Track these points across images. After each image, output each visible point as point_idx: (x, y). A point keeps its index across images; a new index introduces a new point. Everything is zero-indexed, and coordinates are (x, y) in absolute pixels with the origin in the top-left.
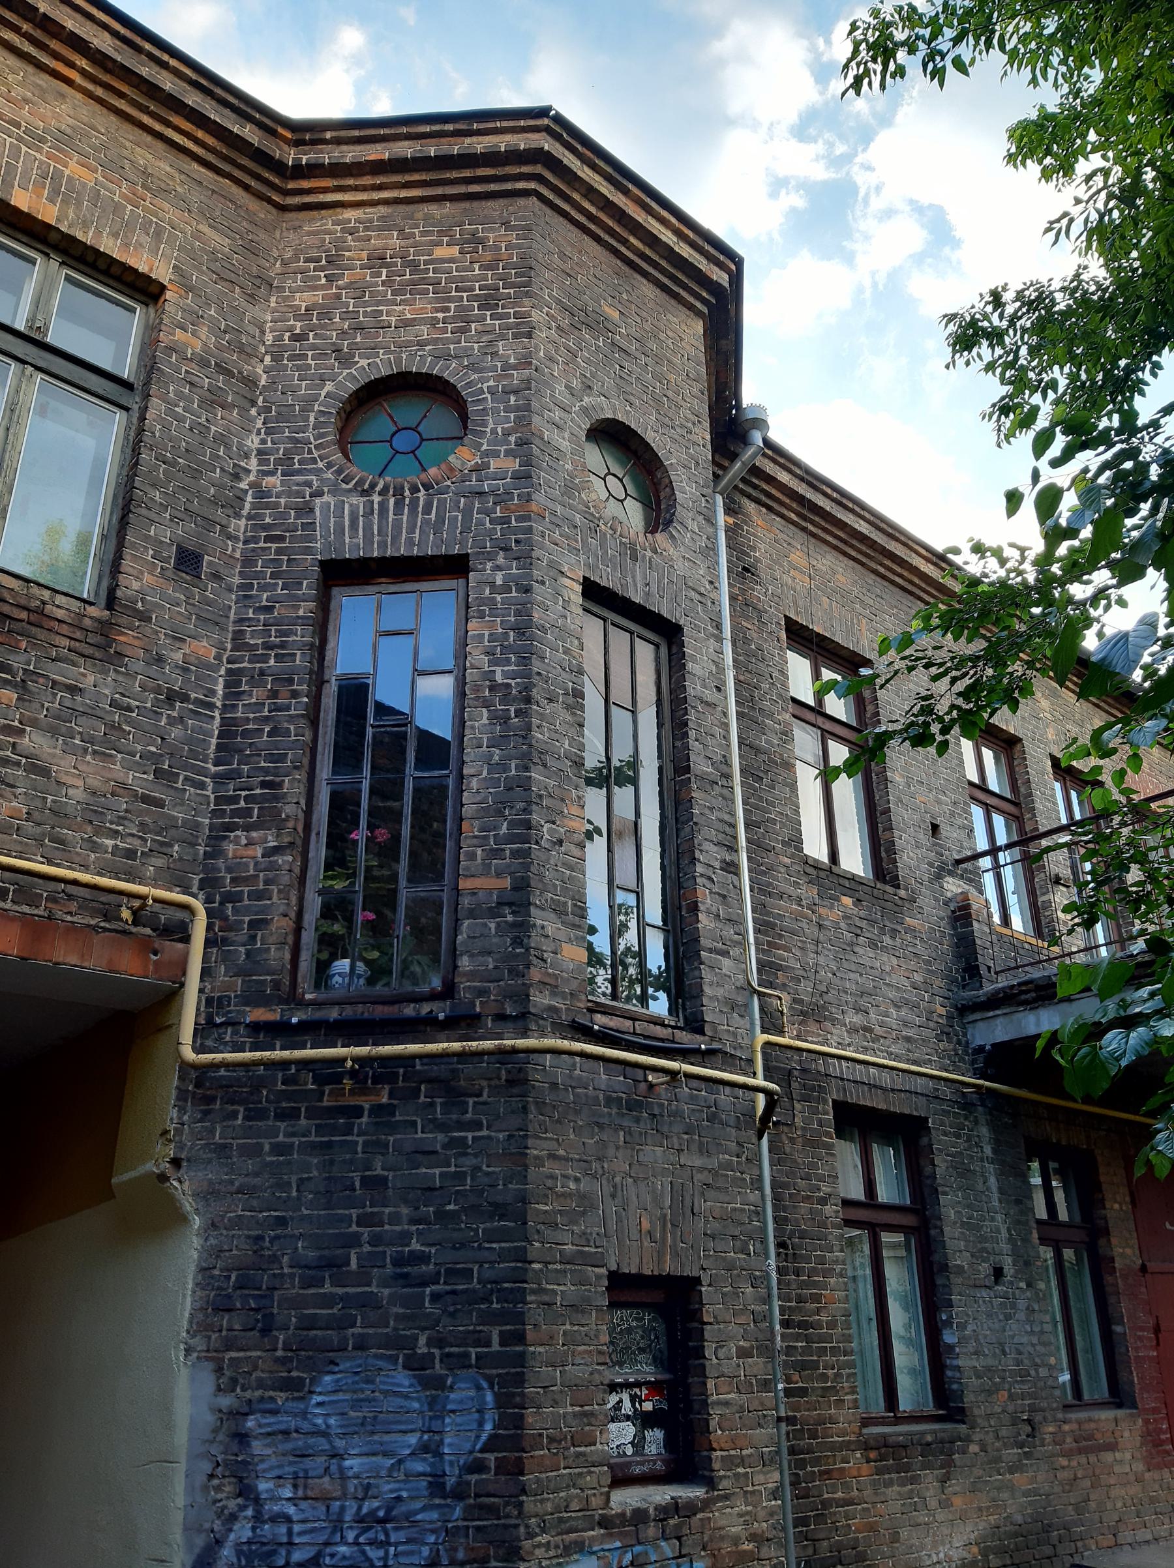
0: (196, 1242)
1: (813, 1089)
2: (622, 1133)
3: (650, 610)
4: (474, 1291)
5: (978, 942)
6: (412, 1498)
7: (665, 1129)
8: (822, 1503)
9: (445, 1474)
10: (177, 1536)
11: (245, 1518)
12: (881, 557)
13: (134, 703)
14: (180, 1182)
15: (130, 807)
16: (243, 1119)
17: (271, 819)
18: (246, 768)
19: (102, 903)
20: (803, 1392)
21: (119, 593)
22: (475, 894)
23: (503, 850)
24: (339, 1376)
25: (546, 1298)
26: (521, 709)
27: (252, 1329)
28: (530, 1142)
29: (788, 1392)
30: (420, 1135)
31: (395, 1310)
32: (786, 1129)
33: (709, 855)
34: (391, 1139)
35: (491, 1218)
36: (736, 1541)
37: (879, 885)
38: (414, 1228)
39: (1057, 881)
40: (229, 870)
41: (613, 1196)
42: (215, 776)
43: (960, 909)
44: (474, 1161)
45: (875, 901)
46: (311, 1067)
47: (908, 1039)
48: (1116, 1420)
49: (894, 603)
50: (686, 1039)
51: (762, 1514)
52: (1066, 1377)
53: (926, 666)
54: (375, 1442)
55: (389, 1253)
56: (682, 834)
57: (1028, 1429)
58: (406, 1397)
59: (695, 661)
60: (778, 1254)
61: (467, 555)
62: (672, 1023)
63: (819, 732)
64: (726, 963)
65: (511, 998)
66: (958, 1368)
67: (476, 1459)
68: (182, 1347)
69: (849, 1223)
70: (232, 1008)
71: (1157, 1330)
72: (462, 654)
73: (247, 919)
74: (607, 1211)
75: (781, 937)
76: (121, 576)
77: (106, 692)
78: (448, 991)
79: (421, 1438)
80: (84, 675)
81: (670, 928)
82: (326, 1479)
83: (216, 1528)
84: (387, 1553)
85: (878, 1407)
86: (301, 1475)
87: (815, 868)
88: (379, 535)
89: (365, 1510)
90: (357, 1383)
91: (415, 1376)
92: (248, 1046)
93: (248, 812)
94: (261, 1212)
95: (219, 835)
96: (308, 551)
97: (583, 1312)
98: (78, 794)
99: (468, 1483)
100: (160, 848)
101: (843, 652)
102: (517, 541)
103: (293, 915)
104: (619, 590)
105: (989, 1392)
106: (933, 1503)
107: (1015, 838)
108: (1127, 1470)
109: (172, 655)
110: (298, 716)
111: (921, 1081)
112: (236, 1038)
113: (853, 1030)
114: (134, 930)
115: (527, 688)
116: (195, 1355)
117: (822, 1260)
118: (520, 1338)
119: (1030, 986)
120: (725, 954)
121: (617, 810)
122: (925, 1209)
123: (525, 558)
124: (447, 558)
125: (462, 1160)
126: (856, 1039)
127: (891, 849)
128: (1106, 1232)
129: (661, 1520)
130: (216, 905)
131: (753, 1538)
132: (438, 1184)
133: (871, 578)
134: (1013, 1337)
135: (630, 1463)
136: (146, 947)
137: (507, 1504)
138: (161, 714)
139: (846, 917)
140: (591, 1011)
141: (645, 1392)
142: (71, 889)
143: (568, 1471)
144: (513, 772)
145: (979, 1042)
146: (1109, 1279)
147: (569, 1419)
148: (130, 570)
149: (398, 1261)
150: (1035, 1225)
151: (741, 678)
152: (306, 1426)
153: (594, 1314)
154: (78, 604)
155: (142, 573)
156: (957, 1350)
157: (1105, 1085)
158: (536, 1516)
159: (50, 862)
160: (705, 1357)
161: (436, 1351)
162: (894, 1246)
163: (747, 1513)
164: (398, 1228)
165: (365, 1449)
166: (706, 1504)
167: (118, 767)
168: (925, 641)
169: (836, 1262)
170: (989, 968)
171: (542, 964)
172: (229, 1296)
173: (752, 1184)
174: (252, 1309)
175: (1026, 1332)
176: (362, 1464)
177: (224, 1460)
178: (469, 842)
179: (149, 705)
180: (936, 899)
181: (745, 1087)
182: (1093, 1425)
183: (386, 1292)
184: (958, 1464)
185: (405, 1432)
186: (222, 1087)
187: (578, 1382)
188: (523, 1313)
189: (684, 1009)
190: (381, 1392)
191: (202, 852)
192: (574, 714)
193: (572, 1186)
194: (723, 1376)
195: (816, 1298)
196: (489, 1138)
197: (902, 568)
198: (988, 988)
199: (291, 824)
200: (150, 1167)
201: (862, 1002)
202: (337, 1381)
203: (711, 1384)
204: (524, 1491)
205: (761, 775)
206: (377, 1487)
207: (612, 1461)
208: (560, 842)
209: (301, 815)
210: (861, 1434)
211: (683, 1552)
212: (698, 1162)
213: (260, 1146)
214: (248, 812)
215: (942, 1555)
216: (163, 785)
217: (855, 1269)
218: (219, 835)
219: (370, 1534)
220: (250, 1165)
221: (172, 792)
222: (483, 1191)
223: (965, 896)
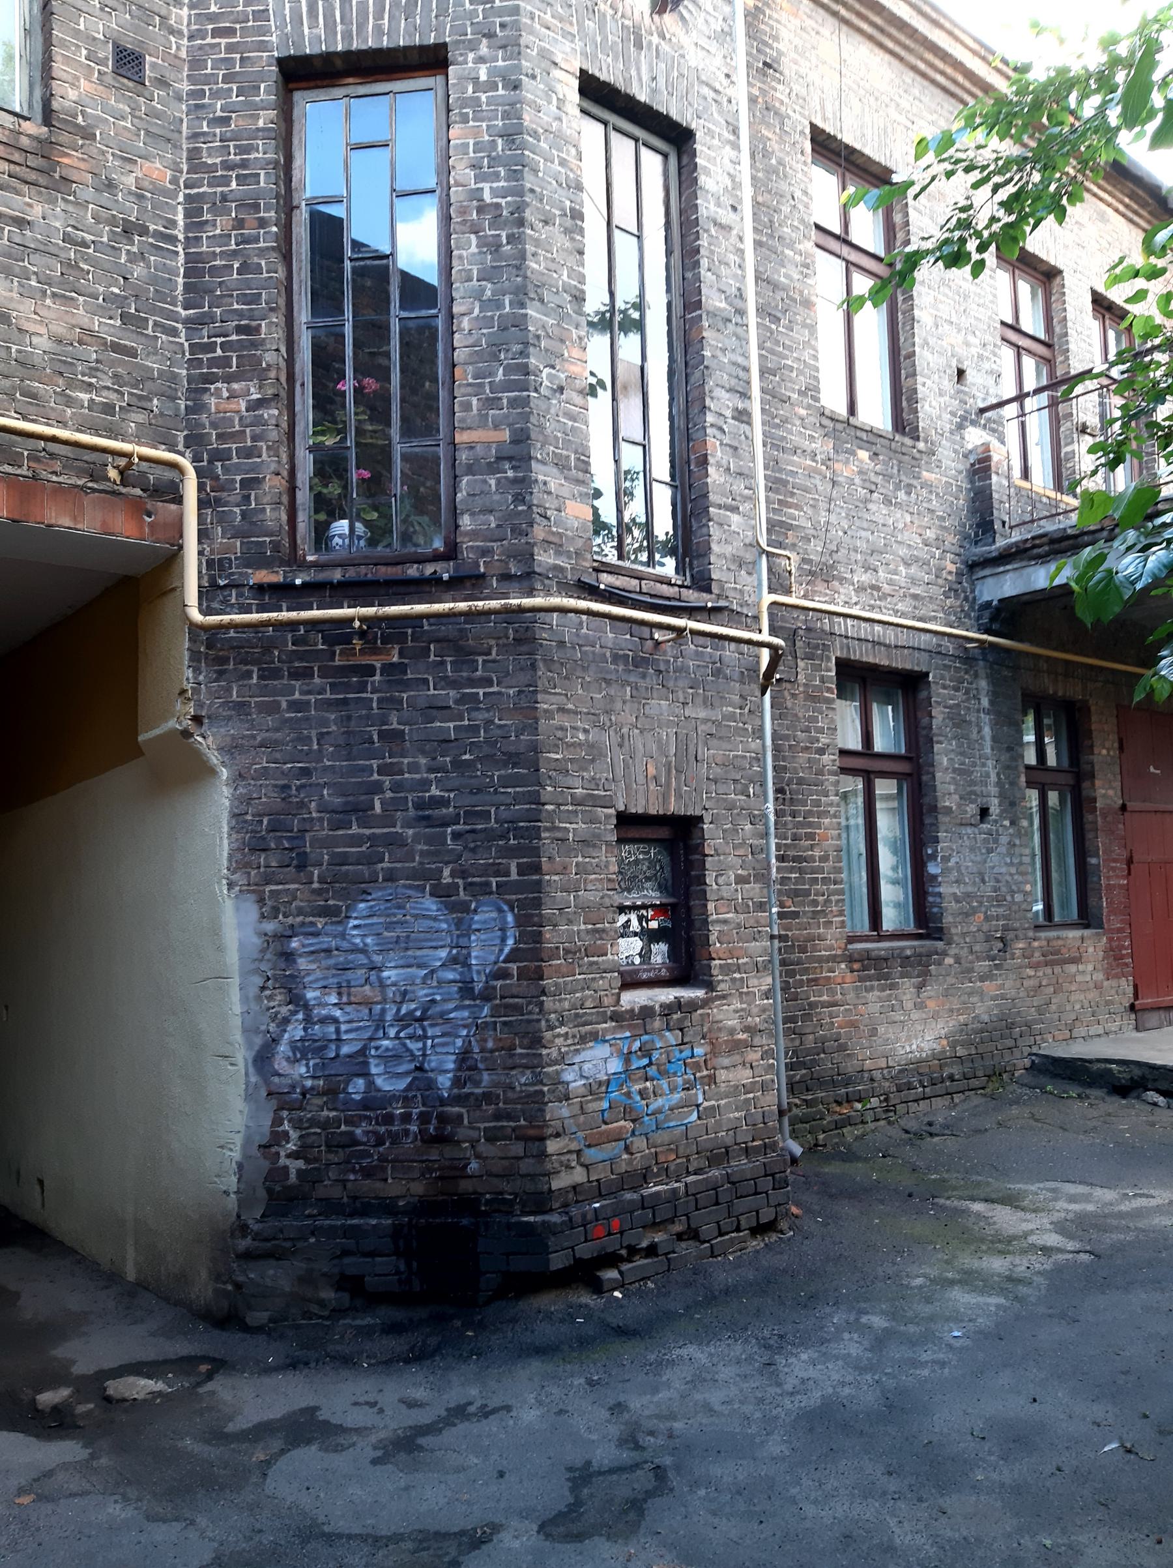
0: (226, 791)
1: (817, 647)
2: (628, 689)
3: (657, 111)
4: (492, 829)
5: (995, 496)
6: (444, 1000)
7: (671, 684)
8: (810, 1004)
9: (473, 981)
10: (238, 1037)
11: (297, 1020)
12: (921, 50)
13: (89, 238)
14: (204, 737)
15: (100, 357)
16: (259, 678)
17: (251, 369)
18: (218, 311)
19: (87, 462)
20: (795, 915)
21: (55, 105)
22: (472, 448)
23: (500, 399)
24: (372, 903)
25: (559, 835)
26: (513, 235)
27: (288, 866)
28: (540, 697)
29: (781, 915)
30: (432, 692)
31: (419, 847)
32: (788, 686)
33: (720, 402)
34: (405, 696)
35: (505, 765)
36: (732, 1031)
37: (897, 437)
38: (433, 776)
39: (1083, 430)
40: (214, 425)
41: (621, 746)
42: (187, 321)
43: (980, 461)
44: (486, 715)
45: (892, 455)
46: (320, 627)
47: (915, 597)
48: (1082, 938)
49: (933, 106)
50: (693, 597)
51: (755, 1011)
52: (1039, 907)
53: (967, 170)
54: (409, 956)
55: (410, 798)
56: (692, 380)
57: (1001, 945)
58: (435, 919)
59: (708, 174)
60: (776, 799)
61: (445, 45)
62: (679, 582)
63: (844, 264)
64: (735, 518)
65: (515, 557)
66: (940, 895)
67: (500, 969)
68: (224, 882)
69: (844, 770)
70: (233, 570)
71: (1130, 861)
72: (445, 169)
73: (238, 478)
74: (615, 760)
75: (792, 494)
76: (54, 83)
77: (58, 224)
78: (451, 552)
79: (450, 952)
80: (30, 205)
81: (678, 483)
82: (367, 987)
83: (271, 1030)
84: (425, 1045)
85: (863, 925)
86: (344, 984)
87: (832, 419)
88: (342, 23)
89: (403, 1011)
90: (389, 908)
91: (441, 902)
92: (254, 607)
93: (225, 362)
94: (285, 763)
95: (199, 387)
96: (263, 46)
97: (594, 846)
98: (43, 343)
99: (494, 988)
100: (139, 404)
101: (873, 169)
102: (503, 26)
103: (285, 473)
104: (620, 85)
105: (967, 915)
106: (909, 1005)
107: (1044, 382)
108: (1088, 978)
109: (124, 179)
110: (267, 248)
111: (925, 637)
112: (241, 600)
113: (861, 589)
114: (124, 490)
115: (519, 208)
116: (238, 888)
117: (817, 803)
118: (537, 868)
119: (1045, 540)
120: (735, 510)
121: (621, 354)
122: (919, 757)
123: (512, 46)
124: (423, 49)
125: (474, 714)
126: (864, 598)
127: (913, 399)
128: (1092, 776)
129: (666, 1015)
130: (205, 463)
131: (747, 1029)
132: (453, 737)
133: (909, 76)
134: (993, 868)
135: (638, 970)
136: (138, 509)
137: (529, 1003)
138: (120, 249)
139: (860, 472)
140: (596, 570)
141: (651, 913)
142: (52, 447)
143: (582, 976)
144: (507, 309)
145: (986, 597)
146: (1089, 817)
147: (583, 935)
148: (64, 76)
149: (419, 806)
150: (1024, 770)
151: (760, 199)
152: (345, 945)
153: (604, 848)
154: (11, 118)
155: (78, 79)
156: (940, 879)
157: (1117, 609)
158: (555, 1012)
159: (25, 418)
160: (705, 884)
161: (460, 882)
162: (887, 798)
163: (742, 1010)
164: (417, 776)
165: (401, 962)
166: (705, 1003)
167: (81, 312)
168: (967, 140)
169: (831, 805)
170: (1004, 523)
171: (545, 522)
172: (263, 838)
173: (753, 733)
174: (286, 849)
175: (1006, 864)
176: (398, 975)
177: (274, 975)
178: (463, 390)
179: (105, 239)
180: (955, 451)
181: (749, 642)
182: (1060, 942)
183: (411, 832)
184: (934, 973)
185: (436, 948)
186: (233, 648)
187: (591, 904)
188: (538, 848)
189: (691, 569)
190: (413, 916)
191: (183, 407)
192: (572, 239)
193: (582, 736)
194: (722, 899)
195: (811, 837)
196: (499, 693)
197: (945, 62)
198: (1001, 543)
199: (273, 374)
200: (172, 724)
201: (871, 560)
202: (371, 907)
203: (711, 906)
204: (544, 993)
205: (779, 315)
206: (413, 992)
207: (622, 969)
208: (561, 389)
209: (283, 364)
210: (846, 949)
211: (685, 1040)
212: (702, 714)
213: (278, 703)
214: (225, 362)
215: (914, 1047)
216: (133, 331)
217: (847, 819)
218: (199, 387)
219: (410, 1030)
220: (270, 721)
221: (143, 340)
222: (496, 742)
223: (987, 448)
